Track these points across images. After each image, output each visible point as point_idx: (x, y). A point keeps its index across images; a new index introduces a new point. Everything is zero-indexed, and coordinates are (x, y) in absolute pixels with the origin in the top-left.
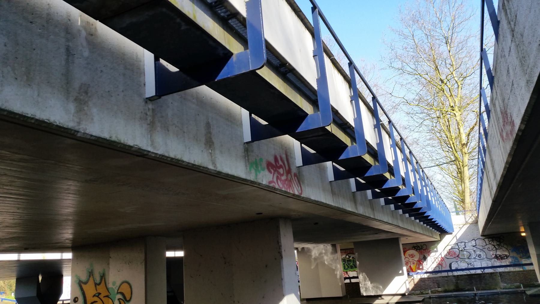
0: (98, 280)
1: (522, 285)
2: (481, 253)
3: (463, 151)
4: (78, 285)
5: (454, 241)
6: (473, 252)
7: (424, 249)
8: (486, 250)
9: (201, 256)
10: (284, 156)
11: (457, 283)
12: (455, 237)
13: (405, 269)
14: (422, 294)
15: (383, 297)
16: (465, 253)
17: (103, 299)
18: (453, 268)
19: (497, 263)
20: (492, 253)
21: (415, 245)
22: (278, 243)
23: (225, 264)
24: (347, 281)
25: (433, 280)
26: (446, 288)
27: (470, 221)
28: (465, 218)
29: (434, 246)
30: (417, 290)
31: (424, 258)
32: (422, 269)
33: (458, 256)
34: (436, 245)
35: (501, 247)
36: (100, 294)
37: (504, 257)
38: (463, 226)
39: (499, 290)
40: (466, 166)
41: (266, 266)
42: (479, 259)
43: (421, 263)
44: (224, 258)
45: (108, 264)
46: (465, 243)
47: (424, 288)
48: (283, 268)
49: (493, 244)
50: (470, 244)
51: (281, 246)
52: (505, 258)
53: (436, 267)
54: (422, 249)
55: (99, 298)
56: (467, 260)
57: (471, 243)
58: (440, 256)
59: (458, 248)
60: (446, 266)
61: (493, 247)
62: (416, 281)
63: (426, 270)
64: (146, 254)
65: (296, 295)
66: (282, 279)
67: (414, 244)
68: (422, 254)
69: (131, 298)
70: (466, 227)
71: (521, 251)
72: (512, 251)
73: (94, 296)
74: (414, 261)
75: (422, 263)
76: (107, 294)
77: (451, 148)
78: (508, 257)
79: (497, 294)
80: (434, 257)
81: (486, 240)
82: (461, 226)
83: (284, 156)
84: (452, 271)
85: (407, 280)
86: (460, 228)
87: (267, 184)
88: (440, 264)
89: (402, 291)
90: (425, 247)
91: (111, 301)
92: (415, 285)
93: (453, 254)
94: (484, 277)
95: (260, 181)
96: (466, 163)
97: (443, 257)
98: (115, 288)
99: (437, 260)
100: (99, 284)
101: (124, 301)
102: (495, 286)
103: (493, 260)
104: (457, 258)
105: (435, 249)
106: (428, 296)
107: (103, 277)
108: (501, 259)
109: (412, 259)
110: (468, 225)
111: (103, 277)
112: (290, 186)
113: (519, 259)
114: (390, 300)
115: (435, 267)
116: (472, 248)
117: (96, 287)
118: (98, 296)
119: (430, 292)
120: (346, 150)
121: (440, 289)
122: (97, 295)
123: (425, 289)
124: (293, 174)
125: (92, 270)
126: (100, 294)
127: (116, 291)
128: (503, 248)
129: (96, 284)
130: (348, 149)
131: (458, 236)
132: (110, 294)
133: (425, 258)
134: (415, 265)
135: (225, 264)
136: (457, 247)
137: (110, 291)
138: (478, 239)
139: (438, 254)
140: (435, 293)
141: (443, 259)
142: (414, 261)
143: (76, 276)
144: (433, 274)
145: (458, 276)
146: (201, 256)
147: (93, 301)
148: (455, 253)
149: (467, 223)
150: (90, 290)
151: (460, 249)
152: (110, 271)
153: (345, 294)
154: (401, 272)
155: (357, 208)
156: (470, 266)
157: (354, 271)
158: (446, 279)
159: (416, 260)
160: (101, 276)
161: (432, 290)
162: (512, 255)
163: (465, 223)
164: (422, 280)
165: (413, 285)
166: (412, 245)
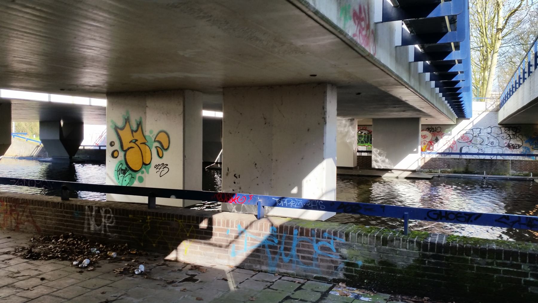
0: (135, 127)
1: (531, 173)
2: (494, 141)
3: (497, 36)
4: (114, 130)
5: (470, 126)
6: (486, 139)
7: (437, 131)
8: (500, 139)
9: (241, 114)
10: (366, 7)
11: (468, 166)
12: (472, 123)
13: (420, 147)
14: (431, 172)
15: (393, 171)
16: (478, 139)
17: (140, 146)
18: (463, 152)
19: (509, 151)
20: (505, 142)
21: (430, 127)
22: (324, 108)
23: (265, 124)
24: (358, 154)
25: (445, 161)
26: (456, 169)
27: (491, 108)
28: (486, 105)
29: (449, 129)
30: (427, 169)
31: (436, 139)
32: (432, 150)
33: (471, 141)
34: (451, 128)
35: (516, 137)
36: (136, 140)
37: (517, 146)
38: (482, 113)
39: (508, 176)
40: (496, 52)
41: (308, 130)
42: (491, 146)
43: (431, 144)
44: (265, 119)
45: (145, 113)
46: (481, 129)
47: (433, 167)
48: (326, 133)
49: (508, 133)
50: (485, 131)
51: (326, 112)
52: (518, 147)
53: (446, 150)
54: (436, 131)
55: (136, 144)
56: (478, 146)
57: (487, 130)
58: (453, 140)
59: (473, 134)
60: (457, 149)
61: (508, 136)
62: (427, 160)
63: (436, 151)
64: (184, 106)
65: (334, 160)
66: (324, 144)
67: (429, 126)
68: (435, 136)
69: (168, 147)
70: (485, 114)
71: (535, 142)
72: (526, 142)
73: (131, 142)
74: (426, 142)
75: (433, 144)
76: (144, 141)
77: (483, 33)
78: (521, 147)
79: (506, 179)
80: (447, 140)
81: (503, 129)
82: (480, 113)
83: (366, 7)
84: (461, 154)
85: (420, 158)
86: (478, 114)
87: (352, 36)
88: (451, 147)
89: (414, 168)
90: (439, 130)
91: (148, 148)
92: (425, 163)
93: (466, 139)
94: (496, 163)
95: (346, 31)
96: (497, 49)
97: (455, 140)
98: (153, 136)
99: (449, 143)
100: (136, 131)
101: (161, 149)
102: (504, 172)
103: (505, 148)
104: (469, 143)
105: (449, 133)
106: (437, 175)
107: (139, 124)
108: (513, 148)
109: (424, 139)
110: (487, 113)
111: (139, 124)
112: (367, 44)
113: (531, 150)
114: (399, 175)
115: (446, 149)
116: (486, 134)
117: (132, 133)
118: (135, 143)
119: (440, 171)
120: (438, 7)
121: (449, 169)
122: (134, 141)
123: (434, 168)
124: (371, 30)
125: (128, 117)
126: (136, 140)
127: (153, 139)
128: (517, 138)
129: (132, 131)
130: (440, 6)
131: (475, 123)
132: (148, 142)
133: (437, 140)
134: (426, 145)
135: (265, 124)
136: (472, 132)
137: (147, 138)
138: (495, 128)
139: (451, 137)
140: (445, 173)
141: (455, 143)
142: (426, 142)
143: (112, 121)
144: (442, 156)
145: (470, 159)
146: (241, 114)
147: (130, 147)
148: (468, 138)
149: (487, 109)
150: (127, 136)
151: (475, 135)
152: (147, 120)
153: (356, 165)
154: (415, 150)
155: (410, 80)
156: (480, 152)
157: (364, 146)
158: (458, 161)
159: (428, 140)
160: (138, 124)
161: (441, 170)
162: (524, 145)
163: (485, 110)
164: (433, 160)
165: (423, 164)
166: (427, 127)
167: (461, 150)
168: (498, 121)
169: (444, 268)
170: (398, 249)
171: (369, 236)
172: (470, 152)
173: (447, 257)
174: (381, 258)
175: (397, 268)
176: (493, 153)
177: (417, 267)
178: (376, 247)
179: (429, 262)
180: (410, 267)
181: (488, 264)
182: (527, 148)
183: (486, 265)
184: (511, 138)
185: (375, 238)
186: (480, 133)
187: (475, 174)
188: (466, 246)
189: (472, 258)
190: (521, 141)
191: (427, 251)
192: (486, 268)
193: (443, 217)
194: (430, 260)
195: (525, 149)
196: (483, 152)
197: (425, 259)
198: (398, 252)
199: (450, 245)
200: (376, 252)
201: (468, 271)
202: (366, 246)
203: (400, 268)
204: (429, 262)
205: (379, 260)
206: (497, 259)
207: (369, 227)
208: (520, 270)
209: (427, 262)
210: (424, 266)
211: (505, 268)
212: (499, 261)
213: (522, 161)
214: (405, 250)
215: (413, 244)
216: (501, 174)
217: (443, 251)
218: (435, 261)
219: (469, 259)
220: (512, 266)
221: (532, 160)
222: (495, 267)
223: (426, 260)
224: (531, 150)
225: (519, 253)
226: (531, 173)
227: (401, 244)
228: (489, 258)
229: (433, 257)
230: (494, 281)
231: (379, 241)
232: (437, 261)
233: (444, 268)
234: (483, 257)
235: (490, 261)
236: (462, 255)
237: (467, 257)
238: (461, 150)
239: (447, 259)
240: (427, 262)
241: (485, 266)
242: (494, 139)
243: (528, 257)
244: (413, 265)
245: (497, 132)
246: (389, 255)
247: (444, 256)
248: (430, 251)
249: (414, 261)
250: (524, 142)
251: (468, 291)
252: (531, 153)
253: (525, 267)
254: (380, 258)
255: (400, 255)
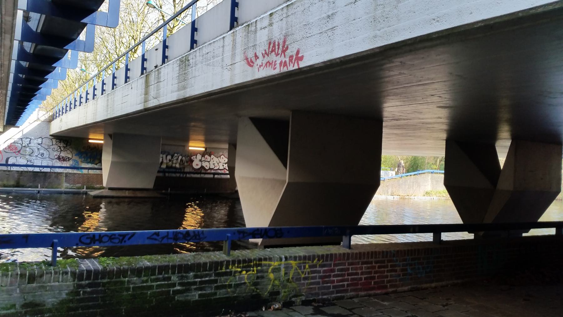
1: (85, 186)
2: (45, 152)
5: (20, 135)
6: (36, 150)
8: (50, 150)
11: (19, 179)
12: (22, 131)
16: (28, 149)
18: (9, 163)
19: (59, 164)
20: (56, 153)
26: (5, 182)
27: (43, 119)
33: (19, 152)
35: (66, 149)
39: (63, 189)
46: (31, 139)
49: (59, 145)
50: (35, 141)
52: (67, 160)
56: (27, 157)
57: (37, 140)
59: (21, 143)
61: (59, 148)
72: (75, 155)
78: (71, 159)
79: (61, 193)
81: (54, 140)
93: (14, 149)
110: (39, 122)
113: (80, 163)
131: (25, 132)
136: (21, 142)
145: (22, 171)
151: (24, 145)
156: (29, 163)
158: (8, 173)
163: (36, 119)
167: (7, 160)
168: (49, 132)
169: (100, 295)
170: (49, 284)
171: (10, 275)
172: (17, 164)
173: (103, 283)
174: (25, 300)
175: (45, 307)
176: (43, 165)
177: (71, 301)
178: (18, 287)
179: (83, 292)
180: (62, 302)
181: (143, 282)
182: (76, 160)
183: (141, 283)
184: (61, 151)
185: (19, 276)
186: (30, 143)
187: (26, 187)
188: (123, 268)
189: (129, 279)
190: (71, 154)
191: (83, 280)
192: (142, 286)
193: (97, 240)
194: (85, 290)
195: (74, 161)
196: (32, 164)
197: (80, 290)
198: (48, 288)
199: (108, 269)
200: (19, 293)
201: (125, 293)
202: (5, 288)
203: (49, 306)
204: (84, 293)
205: (22, 303)
206: (152, 275)
207: (231, 266)
208: (170, 282)
209: (81, 292)
210: (78, 297)
211: (158, 283)
212: (153, 277)
213: (76, 174)
214: (57, 284)
215: (67, 276)
216: (54, 187)
217: (100, 277)
218: (91, 289)
219: (126, 281)
220: (164, 279)
221: (80, 172)
222: (149, 284)
223: (81, 291)
224: (80, 163)
225: (170, 266)
226: (85, 186)
227: (52, 278)
228: (144, 276)
229: (89, 285)
230: (148, 298)
231: (24, 280)
232: (93, 289)
233: (100, 295)
234: (139, 276)
235: (145, 278)
236: (120, 277)
237: (124, 279)
238: (7, 160)
239: (104, 285)
240: (81, 292)
241: (141, 285)
242: (45, 150)
243: (177, 269)
244: (66, 300)
245: (48, 144)
246: (36, 293)
247: (100, 283)
248: (86, 279)
249: (67, 294)
250: (74, 155)
251: (124, 313)
252: (80, 167)
253: (174, 278)
254: (23, 299)
255: (50, 291)
